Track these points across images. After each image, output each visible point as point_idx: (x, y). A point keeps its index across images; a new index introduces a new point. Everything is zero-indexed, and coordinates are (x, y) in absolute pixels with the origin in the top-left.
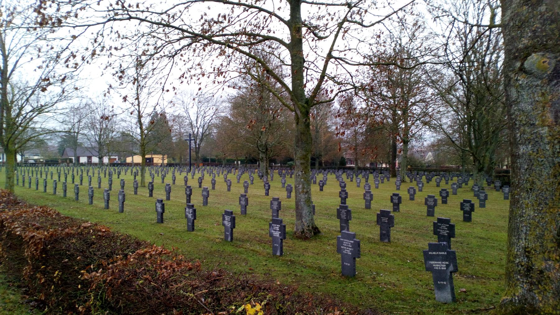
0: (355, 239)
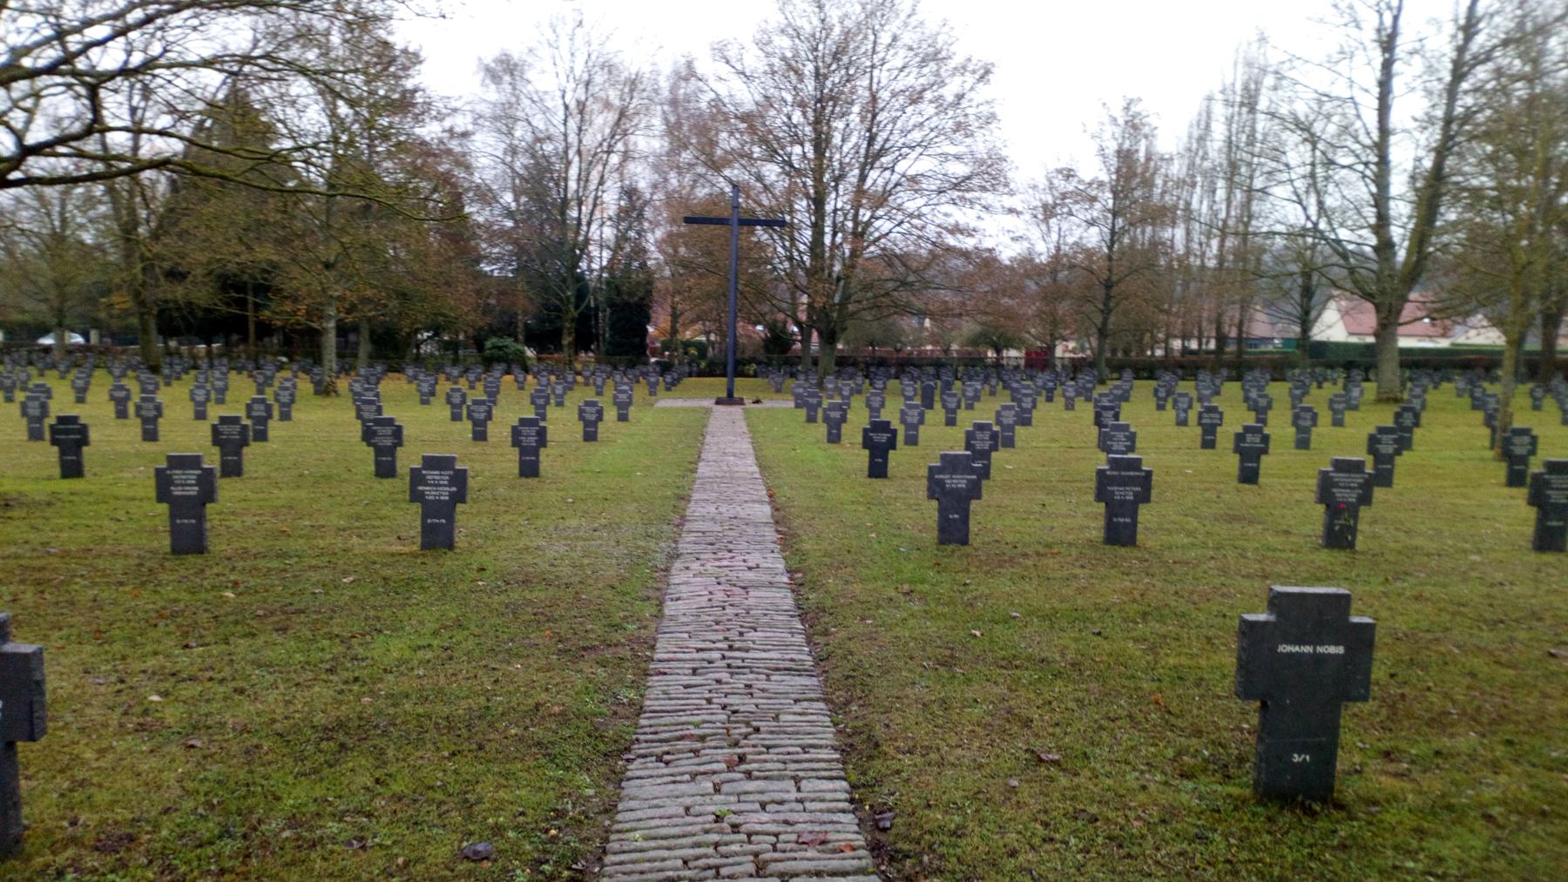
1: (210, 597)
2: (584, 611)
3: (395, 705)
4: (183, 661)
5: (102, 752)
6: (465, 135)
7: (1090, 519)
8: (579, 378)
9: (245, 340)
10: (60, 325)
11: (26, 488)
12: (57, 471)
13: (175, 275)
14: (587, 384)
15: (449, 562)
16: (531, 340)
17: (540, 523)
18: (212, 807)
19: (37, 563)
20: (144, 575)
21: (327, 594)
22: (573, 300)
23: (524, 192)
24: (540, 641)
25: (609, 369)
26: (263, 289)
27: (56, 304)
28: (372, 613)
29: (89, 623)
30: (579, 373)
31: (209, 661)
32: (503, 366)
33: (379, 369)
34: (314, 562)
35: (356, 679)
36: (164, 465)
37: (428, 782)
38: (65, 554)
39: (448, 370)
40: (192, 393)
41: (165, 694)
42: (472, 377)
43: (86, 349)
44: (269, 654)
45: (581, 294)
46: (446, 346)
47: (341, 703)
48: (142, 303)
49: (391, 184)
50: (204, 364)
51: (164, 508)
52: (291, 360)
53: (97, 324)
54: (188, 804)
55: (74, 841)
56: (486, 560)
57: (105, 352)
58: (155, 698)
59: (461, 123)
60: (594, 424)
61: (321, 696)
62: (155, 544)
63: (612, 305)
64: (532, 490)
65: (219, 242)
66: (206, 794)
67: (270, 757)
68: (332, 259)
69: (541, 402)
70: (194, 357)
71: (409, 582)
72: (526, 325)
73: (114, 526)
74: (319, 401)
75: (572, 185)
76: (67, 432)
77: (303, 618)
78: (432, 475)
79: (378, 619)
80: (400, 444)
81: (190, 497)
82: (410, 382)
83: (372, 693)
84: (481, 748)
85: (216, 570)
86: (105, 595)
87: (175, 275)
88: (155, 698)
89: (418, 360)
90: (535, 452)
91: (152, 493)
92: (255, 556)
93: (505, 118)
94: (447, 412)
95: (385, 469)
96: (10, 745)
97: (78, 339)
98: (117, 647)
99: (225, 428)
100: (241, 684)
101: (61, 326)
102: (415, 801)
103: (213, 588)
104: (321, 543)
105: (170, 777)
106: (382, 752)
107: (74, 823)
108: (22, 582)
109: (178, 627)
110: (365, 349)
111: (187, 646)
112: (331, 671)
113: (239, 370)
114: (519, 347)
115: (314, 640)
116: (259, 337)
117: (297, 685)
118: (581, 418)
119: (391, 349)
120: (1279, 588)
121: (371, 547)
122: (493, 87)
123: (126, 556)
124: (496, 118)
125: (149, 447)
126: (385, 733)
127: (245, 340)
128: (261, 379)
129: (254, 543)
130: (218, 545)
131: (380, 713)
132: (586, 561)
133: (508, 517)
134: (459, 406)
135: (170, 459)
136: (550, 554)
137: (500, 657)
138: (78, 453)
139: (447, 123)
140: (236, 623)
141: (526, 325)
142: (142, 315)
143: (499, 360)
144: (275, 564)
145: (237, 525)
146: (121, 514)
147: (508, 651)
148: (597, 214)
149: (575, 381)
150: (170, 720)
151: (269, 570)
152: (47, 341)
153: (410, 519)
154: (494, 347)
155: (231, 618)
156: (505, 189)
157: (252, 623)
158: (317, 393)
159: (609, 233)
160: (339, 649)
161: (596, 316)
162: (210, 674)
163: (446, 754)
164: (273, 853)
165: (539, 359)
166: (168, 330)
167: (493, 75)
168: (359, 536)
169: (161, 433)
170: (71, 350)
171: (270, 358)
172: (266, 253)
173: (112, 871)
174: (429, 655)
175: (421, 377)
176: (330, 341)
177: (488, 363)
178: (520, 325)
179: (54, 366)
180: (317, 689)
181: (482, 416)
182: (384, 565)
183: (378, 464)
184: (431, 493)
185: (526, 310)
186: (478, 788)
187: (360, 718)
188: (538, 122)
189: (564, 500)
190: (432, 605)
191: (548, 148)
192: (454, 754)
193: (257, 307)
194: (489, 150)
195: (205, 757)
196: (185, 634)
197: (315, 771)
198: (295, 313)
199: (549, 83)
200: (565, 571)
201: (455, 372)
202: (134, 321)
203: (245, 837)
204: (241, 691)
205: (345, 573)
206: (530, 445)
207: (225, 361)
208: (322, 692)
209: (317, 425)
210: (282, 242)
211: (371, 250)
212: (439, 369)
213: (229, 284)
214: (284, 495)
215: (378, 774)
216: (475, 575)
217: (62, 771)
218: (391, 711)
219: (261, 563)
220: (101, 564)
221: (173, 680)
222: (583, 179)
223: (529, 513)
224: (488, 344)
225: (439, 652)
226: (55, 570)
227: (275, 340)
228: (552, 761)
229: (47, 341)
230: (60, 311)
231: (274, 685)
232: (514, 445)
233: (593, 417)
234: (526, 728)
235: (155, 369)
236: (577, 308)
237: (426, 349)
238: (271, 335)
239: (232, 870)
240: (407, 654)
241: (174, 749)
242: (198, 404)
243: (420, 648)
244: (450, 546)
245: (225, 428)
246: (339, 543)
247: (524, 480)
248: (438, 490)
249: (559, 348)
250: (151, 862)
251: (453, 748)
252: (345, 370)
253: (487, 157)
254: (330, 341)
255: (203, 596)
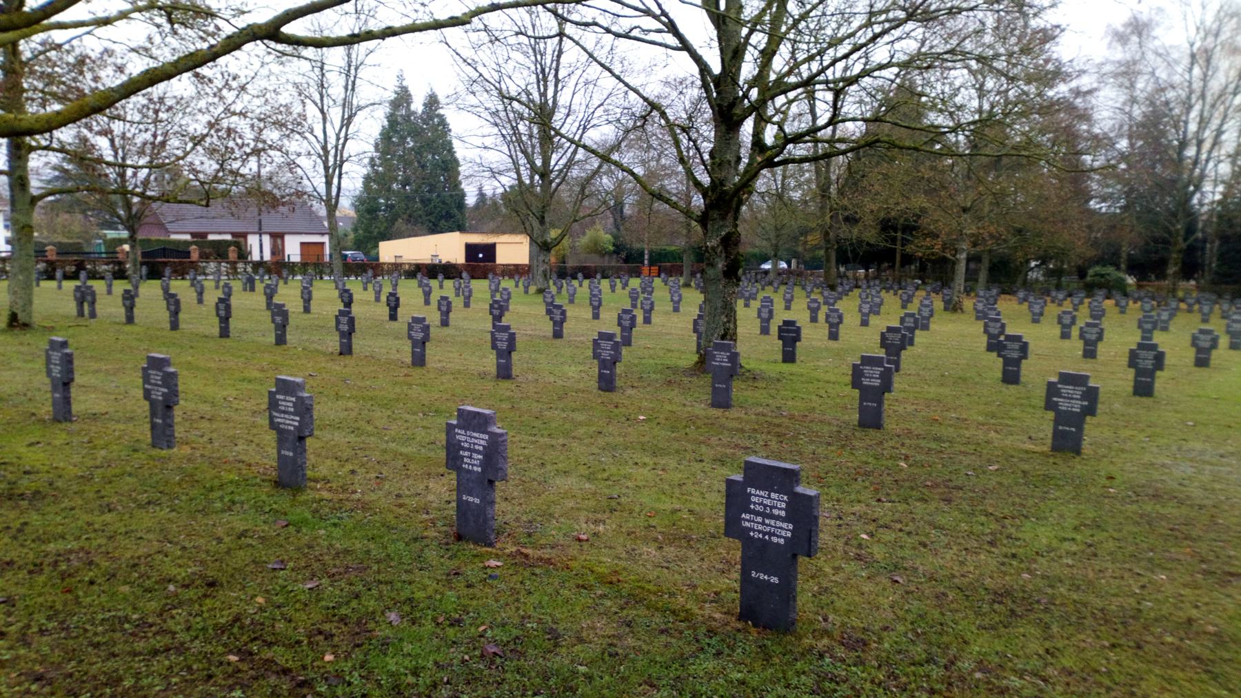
0: (800, 489)
1: (890, 463)
2: (1224, 537)
3: (1052, 587)
4: (879, 511)
5: (837, 569)
6: (1090, 92)
7: (490, 362)
8: (1183, 306)
9: (892, 267)
10: (775, 256)
11: (763, 367)
12: (780, 357)
13: (851, 220)
14: (1190, 311)
15: (1078, 467)
16: (1135, 267)
17: (1162, 441)
18: (918, 635)
19: (776, 421)
20: (842, 441)
21: (977, 477)
22: (1182, 233)
23: (1139, 137)
24: (1181, 557)
25: (1214, 297)
26: (909, 229)
27: (774, 242)
28: (1017, 500)
29: (813, 470)
30: (1182, 300)
31: (897, 516)
32: (1102, 292)
33: (994, 291)
34: (963, 449)
35: (1014, 556)
36: (1054, 379)
37: (1093, 664)
38: (792, 417)
39: (1054, 294)
40: (860, 307)
41: (871, 535)
42: (1076, 301)
43: (789, 272)
44: (942, 520)
45: (1190, 230)
46: (1050, 273)
47: (1005, 573)
48: (828, 241)
49: (1032, 137)
50: (863, 284)
51: (856, 393)
52: (924, 283)
53: (796, 255)
54: (901, 628)
55: (826, 633)
56: (1113, 470)
57: (800, 274)
58: (865, 536)
59: (1085, 82)
60: (1208, 351)
61: (987, 564)
62: (846, 417)
63: (1224, 239)
64: (1149, 409)
65: (885, 195)
66: (912, 623)
67: (954, 606)
68: (969, 204)
69: (1148, 326)
70: (857, 279)
71: (1047, 478)
72: (1129, 255)
73: (820, 401)
74: (948, 316)
75: (1193, 127)
76: (788, 331)
77: (961, 494)
78: (1067, 389)
79: (1024, 506)
80: (1025, 357)
81: (874, 387)
82: (1020, 303)
83: (1029, 571)
84: (1139, 647)
85: (891, 443)
86: (820, 450)
87: (851, 220)
88: (865, 536)
89: (1028, 286)
90: (1151, 374)
91: (848, 379)
92: (918, 436)
93: (1127, 73)
94: (1057, 331)
95: (1011, 376)
96: (795, 556)
97: (784, 265)
98: (833, 491)
99: (890, 336)
100: (923, 539)
101: (776, 257)
102: (1085, 680)
103: (891, 457)
104: (967, 433)
105: (885, 602)
106: (1047, 627)
107: (825, 620)
108: (769, 433)
109: (872, 483)
110: (983, 276)
111: (879, 500)
112: (991, 543)
113: (888, 290)
114: (1121, 275)
115: (973, 514)
116: (903, 265)
117: (966, 549)
118: (1194, 344)
119: (1003, 274)
120: (753, 459)
121: (1008, 442)
122: (1120, 48)
123: (829, 424)
124: (1116, 75)
125: (832, 344)
126: (1046, 610)
127: (892, 267)
128: (905, 297)
129: (917, 427)
130: (890, 424)
131: (1039, 591)
132: (1217, 486)
133: (1128, 433)
134: (1070, 326)
135: (863, 358)
136: (1177, 473)
137: (1143, 563)
138: (794, 347)
139: (1074, 84)
140: (912, 489)
141: (1129, 255)
142: (827, 249)
143: (1100, 286)
144: (933, 445)
145: (901, 410)
146: (822, 392)
147: (1150, 560)
148: (1215, 154)
149: (1177, 309)
150: (877, 556)
151: (930, 449)
152: (767, 266)
153: (1045, 425)
154: (1096, 275)
155: (907, 484)
156: (1121, 136)
157: (924, 490)
158: (946, 309)
159: (1225, 169)
160: (994, 526)
161: (1203, 249)
162: (899, 526)
163: (1107, 644)
164: (970, 688)
165: (1139, 287)
166: (843, 259)
167: (1122, 38)
168: (996, 432)
169: (1099, 353)
170: (780, 273)
171: (909, 280)
172: (919, 201)
173: (855, 665)
174: (1074, 548)
175: (1031, 299)
176: (961, 268)
177: (1090, 289)
178: (1124, 255)
179: (771, 283)
180: (982, 557)
181: (1094, 337)
182: (1021, 460)
183: (1005, 372)
184: (1064, 405)
185: (1130, 243)
186: (1143, 684)
187: (1024, 592)
188: (1162, 74)
189: (1183, 422)
190: (1068, 502)
191: (1171, 94)
192: (1113, 646)
193: (905, 242)
194: (1110, 103)
195: (907, 593)
196: (876, 490)
197: (993, 628)
198: (933, 247)
199: (1175, 36)
200: (1196, 492)
201: (1061, 296)
202: (822, 252)
203: (946, 667)
204: (925, 546)
205: (990, 463)
206: (1146, 368)
207: (877, 282)
208: (988, 561)
209: (952, 336)
210: (929, 192)
211: (999, 198)
212: (1047, 292)
213: (887, 226)
214: (933, 391)
215: (1047, 644)
216: (1104, 481)
217: (812, 577)
218: (1049, 591)
219: (923, 443)
220: (815, 428)
221: (874, 524)
222: (1203, 122)
223: (1149, 431)
224: (1091, 272)
225: (1083, 547)
226: (787, 427)
227: (913, 267)
228: (1215, 679)
229: (767, 266)
230: (776, 246)
231: (948, 546)
232: (1130, 366)
233: (1207, 345)
234: (1182, 640)
235: (832, 288)
236: (1185, 240)
237: (1032, 275)
238: (910, 263)
239: (940, 692)
240: (1055, 543)
241: (885, 581)
242: (863, 314)
243: (1065, 539)
244: (1077, 451)
245: (890, 336)
246: (980, 434)
247: (1138, 398)
248: (1072, 402)
249: (1162, 276)
250: (880, 666)
251: (1113, 640)
252: (968, 291)
253: (1107, 110)
254: (961, 268)
255: (884, 462)
